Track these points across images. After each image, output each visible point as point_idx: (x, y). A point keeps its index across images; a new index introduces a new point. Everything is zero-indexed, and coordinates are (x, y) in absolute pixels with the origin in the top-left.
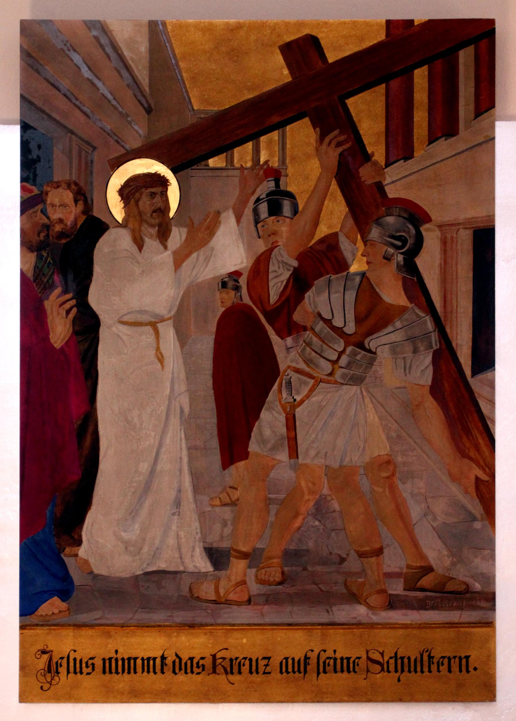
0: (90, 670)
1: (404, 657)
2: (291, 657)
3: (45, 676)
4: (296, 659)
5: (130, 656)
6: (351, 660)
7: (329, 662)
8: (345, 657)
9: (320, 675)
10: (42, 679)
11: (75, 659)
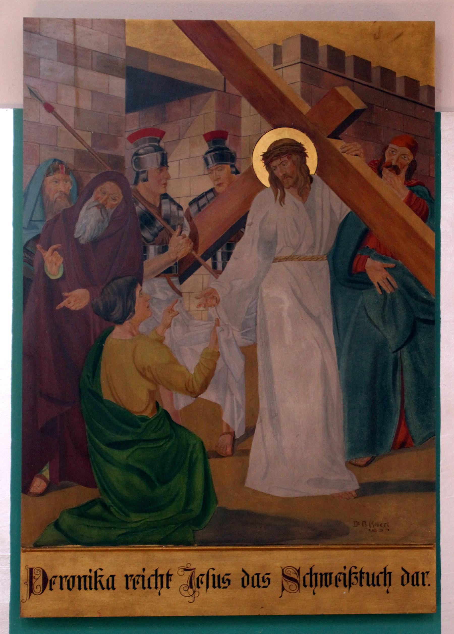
0: (226, 585)
1: (318, 573)
2: (421, 572)
6: (333, 576)
7: (340, 576)
8: (129, 575)
9: (209, 589)
11: (214, 575)
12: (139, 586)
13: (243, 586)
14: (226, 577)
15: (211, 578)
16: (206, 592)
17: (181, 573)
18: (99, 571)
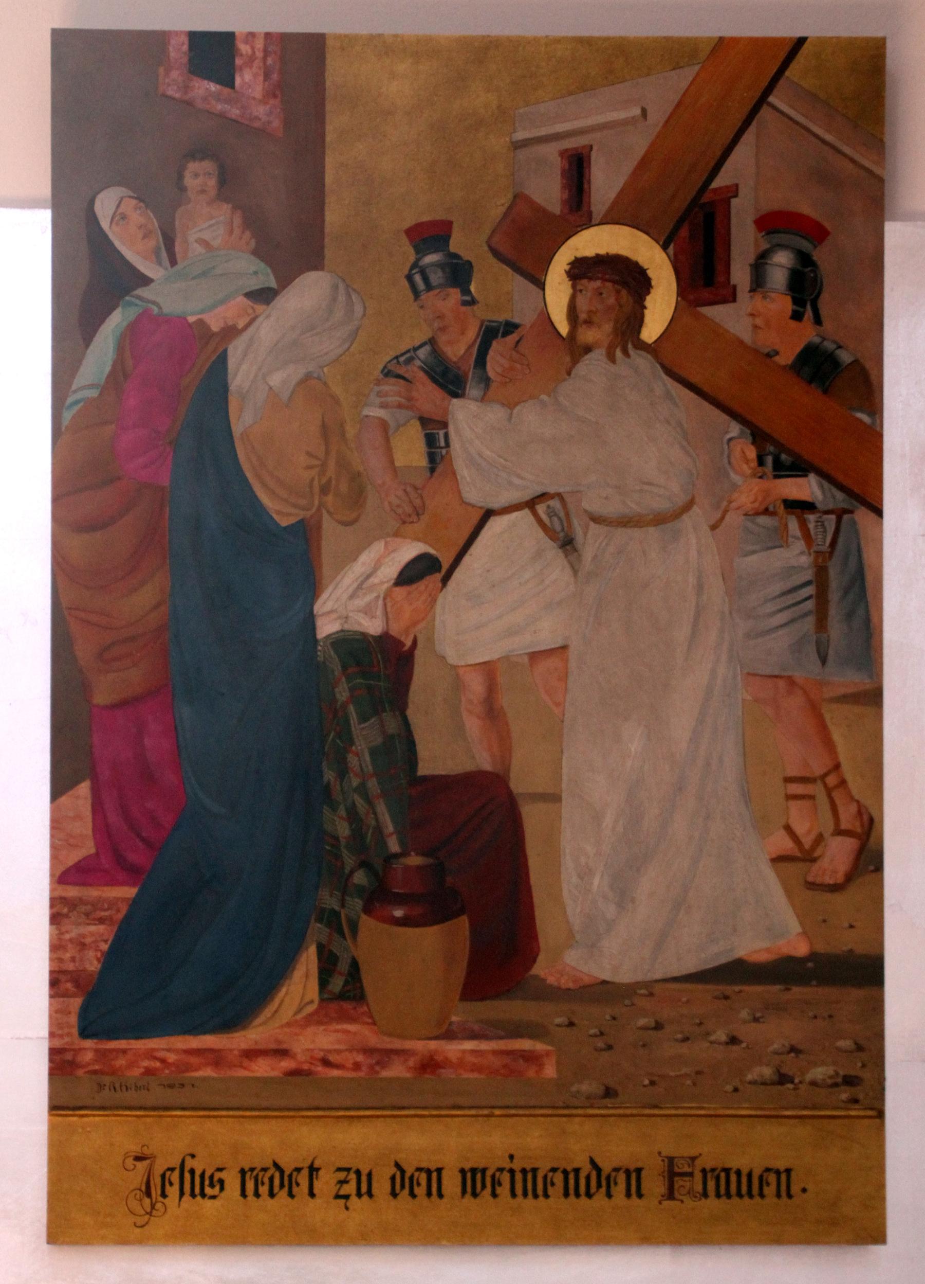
0: (216, 1190)
3: (141, 1200)
4: (745, 1172)
5: (475, 1166)
6: (489, 1173)
9: (184, 1199)
10: (134, 1204)
12: (420, 1191)
13: (394, 1194)
14: (218, 1176)
15: (187, 1176)
16: (179, 1205)
17: (130, 1162)
18: (188, 1159)
